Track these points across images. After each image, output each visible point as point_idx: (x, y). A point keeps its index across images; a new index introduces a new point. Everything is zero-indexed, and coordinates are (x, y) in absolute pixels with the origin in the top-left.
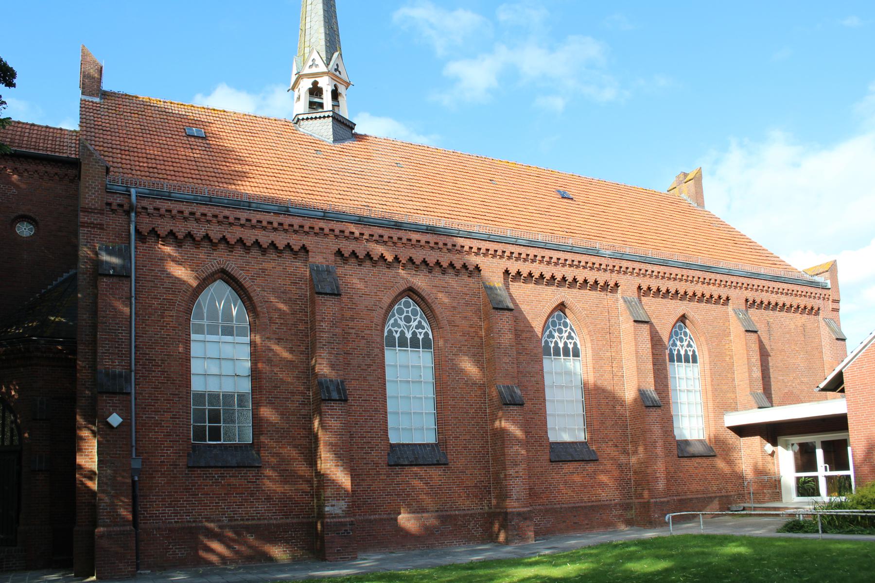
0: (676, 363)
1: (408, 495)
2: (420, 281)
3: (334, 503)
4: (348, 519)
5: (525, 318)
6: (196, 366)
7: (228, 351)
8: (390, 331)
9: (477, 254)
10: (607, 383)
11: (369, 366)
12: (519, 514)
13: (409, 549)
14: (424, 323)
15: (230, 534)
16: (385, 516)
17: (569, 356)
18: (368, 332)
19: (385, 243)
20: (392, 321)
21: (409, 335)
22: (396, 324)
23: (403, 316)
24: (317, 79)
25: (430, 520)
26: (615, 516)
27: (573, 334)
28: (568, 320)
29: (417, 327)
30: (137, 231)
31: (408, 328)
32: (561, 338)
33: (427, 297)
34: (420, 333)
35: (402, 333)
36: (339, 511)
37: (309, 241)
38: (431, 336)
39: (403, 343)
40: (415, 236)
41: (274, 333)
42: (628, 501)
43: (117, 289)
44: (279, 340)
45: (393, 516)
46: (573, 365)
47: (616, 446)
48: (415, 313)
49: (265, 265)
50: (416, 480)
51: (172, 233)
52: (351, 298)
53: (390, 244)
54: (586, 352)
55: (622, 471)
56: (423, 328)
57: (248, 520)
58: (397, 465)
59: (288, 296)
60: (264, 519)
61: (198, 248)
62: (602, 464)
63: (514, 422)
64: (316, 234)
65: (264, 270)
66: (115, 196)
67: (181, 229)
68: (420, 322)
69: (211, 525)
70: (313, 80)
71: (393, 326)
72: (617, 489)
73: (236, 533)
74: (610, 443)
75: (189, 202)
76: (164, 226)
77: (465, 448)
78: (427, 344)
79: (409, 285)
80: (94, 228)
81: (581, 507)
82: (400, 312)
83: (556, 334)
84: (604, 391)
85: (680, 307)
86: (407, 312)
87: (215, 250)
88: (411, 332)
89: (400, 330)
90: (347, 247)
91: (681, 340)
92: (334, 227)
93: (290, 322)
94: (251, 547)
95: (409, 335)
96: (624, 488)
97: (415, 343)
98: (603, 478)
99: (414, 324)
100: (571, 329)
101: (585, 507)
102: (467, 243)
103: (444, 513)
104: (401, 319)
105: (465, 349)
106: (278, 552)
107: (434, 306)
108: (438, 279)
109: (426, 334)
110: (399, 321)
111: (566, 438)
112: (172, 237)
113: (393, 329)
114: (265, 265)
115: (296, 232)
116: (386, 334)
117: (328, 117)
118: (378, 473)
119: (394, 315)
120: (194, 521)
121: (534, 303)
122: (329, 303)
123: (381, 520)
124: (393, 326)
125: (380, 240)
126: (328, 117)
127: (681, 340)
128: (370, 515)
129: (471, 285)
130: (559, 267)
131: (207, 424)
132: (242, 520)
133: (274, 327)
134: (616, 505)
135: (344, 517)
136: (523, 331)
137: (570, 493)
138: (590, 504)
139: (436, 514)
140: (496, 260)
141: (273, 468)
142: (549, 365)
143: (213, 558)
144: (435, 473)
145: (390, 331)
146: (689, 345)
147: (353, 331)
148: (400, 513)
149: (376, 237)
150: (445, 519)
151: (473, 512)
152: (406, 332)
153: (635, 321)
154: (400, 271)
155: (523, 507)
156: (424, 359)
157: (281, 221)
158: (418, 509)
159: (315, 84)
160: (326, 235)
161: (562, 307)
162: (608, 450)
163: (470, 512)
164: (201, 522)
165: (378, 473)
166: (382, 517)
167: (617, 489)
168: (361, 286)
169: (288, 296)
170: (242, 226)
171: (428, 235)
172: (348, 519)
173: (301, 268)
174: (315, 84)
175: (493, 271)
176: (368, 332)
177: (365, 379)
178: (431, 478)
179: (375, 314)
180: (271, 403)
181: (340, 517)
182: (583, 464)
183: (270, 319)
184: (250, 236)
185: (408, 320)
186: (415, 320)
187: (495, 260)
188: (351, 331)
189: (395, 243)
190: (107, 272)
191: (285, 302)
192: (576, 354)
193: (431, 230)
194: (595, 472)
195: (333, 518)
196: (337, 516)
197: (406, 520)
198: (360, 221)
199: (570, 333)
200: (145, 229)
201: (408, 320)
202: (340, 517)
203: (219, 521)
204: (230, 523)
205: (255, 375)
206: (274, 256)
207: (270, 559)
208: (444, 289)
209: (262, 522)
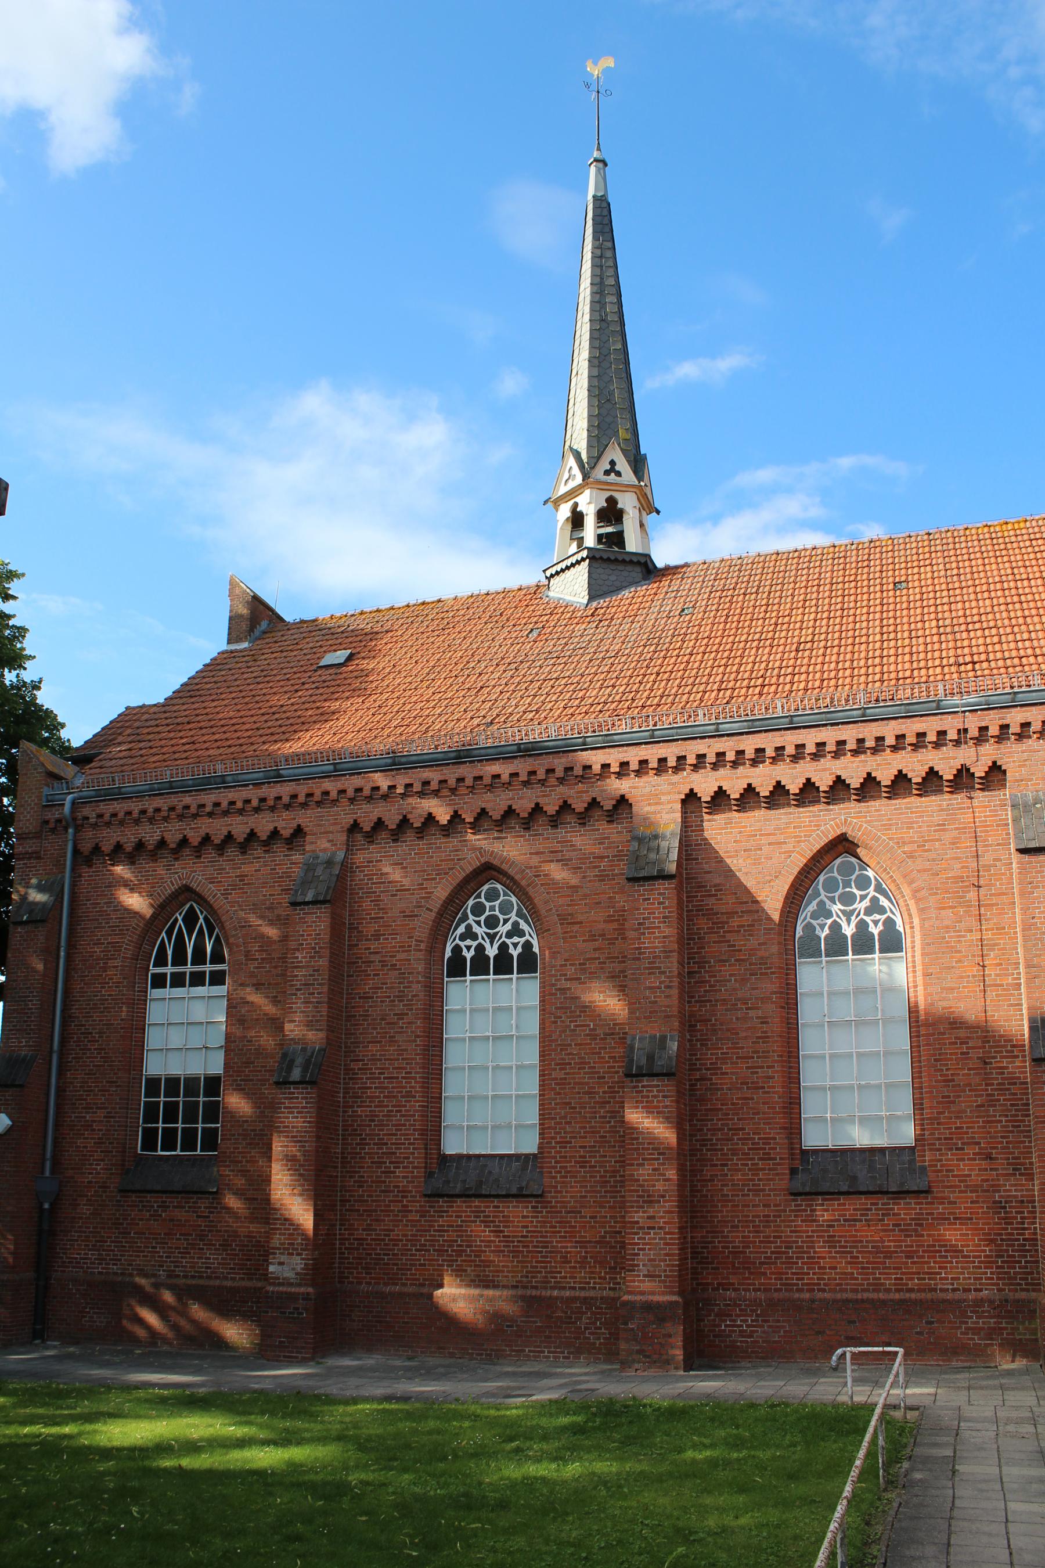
0: (469, 978)
1: (459, 1253)
2: (511, 849)
3: (283, 1258)
4: (302, 1290)
5: (740, 885)
6: (153, 1038)
7: (199, 1012)
8: (457, 950)
9: (619, 775)
10: (967, 1005)
11: (401, 1016)
12: (649, 1307)
13: (452, 1355)
14: (523, 926)
15: (168, 1297)
16: (411, 1290)
17: (871, 951)
18: (403, 956)
19: (436, 793)
20: (462, 929)
21: (492, 952)
22: (469, 934)
23: (482, 918)
24: (616, 495)
25: (501, 1300)
26: (976, 1331)
27: (884, 902)
28: (870, 873)
29: (869, 911)
30: (76, 851)
31: (492, 938)
32: (848, 915)
33: (517, 877)
34: (469, 948)
35: (480, 949)
36: (289, 1274)
37: (304, 818)
38: (536, 949)
39: (480, 965)
40: (503, 769)
41: (252, 975)
42: (1023, 1295)
43: (32, 940)
44: (258, 986)
45: (425, 1290)
46: (896, 973)
47: (989, 1157)
48: (505, 909)
49: (246, 869)
50: (478, 1227)
51: (118, 847)
52: (377, 901)
53: (445, 792)
54: (913, 938)
55: (1008, 1220)
56: (521, 934)
57: (193, 1277)
58: (441, 1196)
59: (276, 912)
60: (217, 1278)
61: (448, 836)
62: (942, 1200)
63: (650, 1109)
64: (319, 803)
65: (242, 877)
66: (54, 809)
67: (129, 837)
68: (516, 924)
69: (142, 1281)
70: (608, 494)
71: (463, 938)
72: (988, 1263)
73: (179, 1298)
74: (969, 1151)
75: (139, 796)
76: (109, 838)
77: (583, 1164)
78: (528, 963)
79: (483, 860)
80: (30, 858)
81: (872, 1301)
82: (478, 910)
83: (837, 908)
84: (955, 1023)
85: (822, 823)
86: (492, 909)
87: (177, 859)
88: (496, 946)
89: (475, 944)
90: (368, 814)
91: (848, 899)
92: (249, 797)
93: (275, 955)
94: (193, 1321)
95: (492, 952)
96: (1011, 1262)
97: (503, 964)
98: (952, 1235)
99: (503, 929)
100: (879, 889)
101: (884, 1302)
102: (596, 759)
103: (529, 1292)
104: (478, 923)
105: (593, 966)
106: (235, 1333)
107: (531, 891)
108: (546, 837)
109: (528, 945)
110: (476, 928)
111: (861, 1137)
112: (117, 853)
113: (462, 944)
114: (246, 869)
115: (287, 807)
116: (448, 954)
117: (583, 559)
118: (405, 1210)
119: (465, 917)
120: (122, 1274)
121: (760, 853)
122: (310, 918)
123: (401, 1295)
124: (463, 938)
125: (426, 790)
126: (583, 559)
127: (848, 899)
128: (386, 1284)
129: (615, 837)
130: (947, 750)
131: (160, 1125)
132: (185, 1277)
133: (252, 966)
134: (978, 1303)
135: (299, 1285)
136: (731, 914)
137: (842, 1265)
138: (897, 1296)
139: (510, 1292)
140: (670, 777)
141: (239, 1193)
142: (811, 976)
143: (141, 1333)
144: (518, 1213)
145: (457, 950)
146: (875, 907)
147: (377, 958)
148: (441, 1286)
149: (417, 787)
150: (532, 1304)
151: (592, 1293)
152: (487, 945)
153: (1022, 851)
154: (470, 837)
155: (663, 1293)
156: (520, 996)
157: (263, 795)
158: (481, 1279)
159: (611, 501)
160: (335, 802)
161: (842, 845)
162: (964, 1168)
163: (583, 1294)
164: (131, 1275)
165: (405, 1210)
166: (405, 1290)
167: (988, 1263)
168: (396, 875)
169: (276, 912)
170: (210, 815)
171: (516, 761)
172: (302, 1290)
173: (292, 863)
174: (611, 501)
175: (658, 802)
176: (403, 956)
177: (392, 1041)
178: (506, 1221)
179: (416, 922)
180: (239, 1089)
181: (291, 1285)
182: (882, 1201)
183: (247, 954)
184: (218, 828)
185: (492, 922)
186: (506, 921)
187: (664, 778)
188: (372, 958)
189: (453, 791)
190: (19, 920)
191: (271, 923)
192: (892, 942)
193: (528, 750)
194: (919, 1221)
195: (280, 1284)
196: (287, 1283)
197: (455, 1296)
198: (395, 763)
199: (874, 900)
200: (86, 847)
201: (492, 922)
202: (291, 1285)
203: (154, 1275)
204: (170, 1281)
205: (231, 1045)
206: (259, 851)
207: (219, 1343)
208: (556, 856)
209: (212, 1283)
